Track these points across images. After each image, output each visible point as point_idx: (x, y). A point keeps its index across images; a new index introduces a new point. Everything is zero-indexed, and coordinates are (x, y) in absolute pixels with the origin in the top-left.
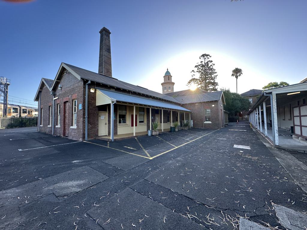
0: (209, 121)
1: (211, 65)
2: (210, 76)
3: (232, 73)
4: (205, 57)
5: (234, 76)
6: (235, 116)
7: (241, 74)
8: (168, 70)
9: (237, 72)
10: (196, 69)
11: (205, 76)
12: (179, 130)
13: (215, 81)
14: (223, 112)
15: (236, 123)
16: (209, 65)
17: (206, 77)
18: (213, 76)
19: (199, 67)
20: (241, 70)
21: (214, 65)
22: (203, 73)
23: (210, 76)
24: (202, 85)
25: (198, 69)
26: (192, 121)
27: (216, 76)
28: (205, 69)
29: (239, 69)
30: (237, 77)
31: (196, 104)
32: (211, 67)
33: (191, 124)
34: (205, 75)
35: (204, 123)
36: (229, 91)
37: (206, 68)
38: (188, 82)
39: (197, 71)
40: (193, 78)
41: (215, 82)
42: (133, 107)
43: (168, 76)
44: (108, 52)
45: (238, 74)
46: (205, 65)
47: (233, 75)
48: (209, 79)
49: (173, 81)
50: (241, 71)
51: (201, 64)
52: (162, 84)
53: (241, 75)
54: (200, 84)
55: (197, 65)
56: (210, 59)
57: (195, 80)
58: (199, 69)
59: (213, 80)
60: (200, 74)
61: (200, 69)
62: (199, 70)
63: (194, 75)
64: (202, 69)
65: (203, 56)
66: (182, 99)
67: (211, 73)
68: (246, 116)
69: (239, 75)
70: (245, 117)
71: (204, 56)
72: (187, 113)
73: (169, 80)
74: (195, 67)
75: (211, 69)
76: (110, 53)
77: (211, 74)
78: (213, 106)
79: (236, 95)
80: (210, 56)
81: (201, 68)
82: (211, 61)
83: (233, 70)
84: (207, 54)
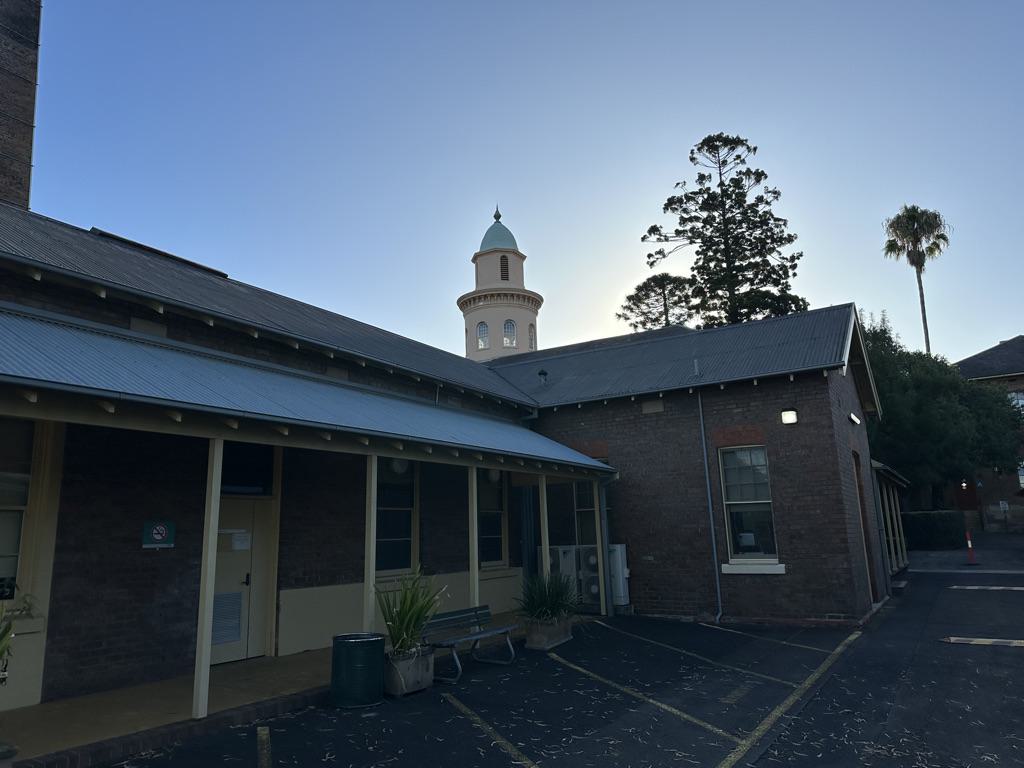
0: (764, 548)
1: (760, 199)
2: (758, 259)
3: (885, 238)
4: (723, 152)
5: (904, 257)
6: (935, 507)
7: (942, 243)
8: (497, 216)
9: (915, 232)
10: (670, 222)
11: (730, 262)
12: (444, 667)
13: (787, 287)
14: (866, 471)
15: (958, 555)
16: (750, 200)
17: (731, 267)
18: (774, 260)
19: (691, 206)
20: (935, 216)
21: (776, 194)
22: (718, 244)
23: (758, 259)
24: (714, 313)
25: (683, 221)
26: (620, 550)
27: (793, 258)
28: (727, 222)
29: (924, 213)
30: (917, 260)
31: (649, 409)
32: (762, 208)
33: (610, 576)
34: (725, 252)
35: (726, 569)
36: (884, 332)
37: (729, 215)
38: (630, 298)
39: (678, 233)
40: (658, 271)
41: (792, 292)
42: (362, 461)
43: (500, 256)
44: (16, 38)
45: (924, 245)
46: (725, 193)
47: (892, 247)
48: (751, 281)
49: (530, 284)
50: (939, 226)
51: (700, 192)
52: (465, 303)
53: (938, 246)
54: (697, 308)
55: (679, 193)
56: (753, 163)
57: (669, 287)
58: (691, 219)
59: (776, 283)
60: (696, 247)
61: (697, 219)
62: (688, 226)
63: (660, 252)
64: (706, 222)
65: (711, 144)
66: (543, 373)
67: (762, 241)
68: (1004, 506)
69: (931, 250)
70: (992, 508)
71: (716, 148)
72: (569, 486)
73: (505, 276)
74: (666, 207)
75: (765, 219)
76: (36, 46)
77: (762, 247)
78: (789, 417)
79: (922, 361)
80: (751, 144)
81: (704, 214)
82: (759, 176)
83: (892, 217)
84: (733, 135)
